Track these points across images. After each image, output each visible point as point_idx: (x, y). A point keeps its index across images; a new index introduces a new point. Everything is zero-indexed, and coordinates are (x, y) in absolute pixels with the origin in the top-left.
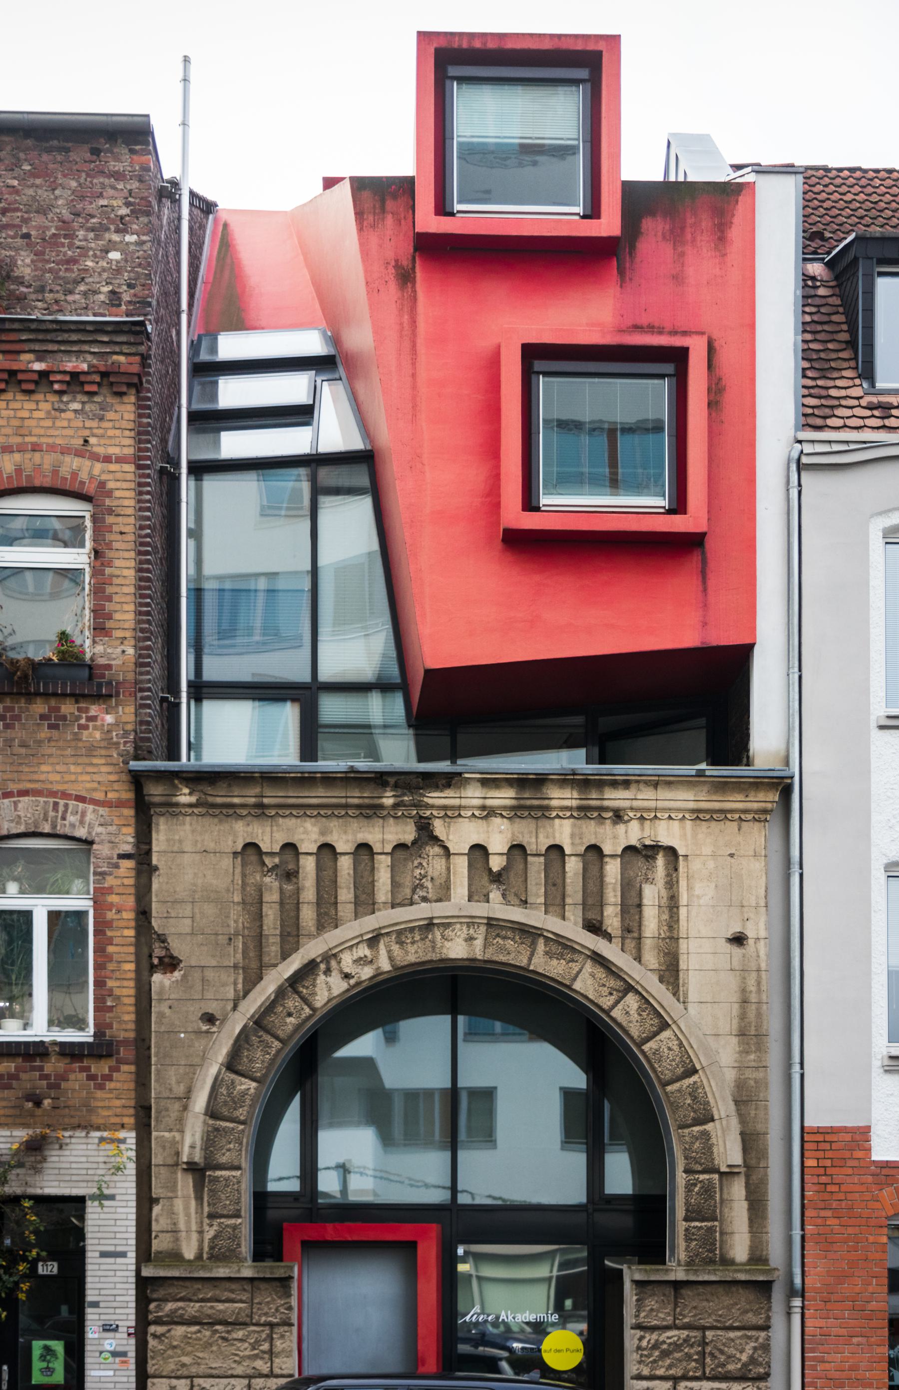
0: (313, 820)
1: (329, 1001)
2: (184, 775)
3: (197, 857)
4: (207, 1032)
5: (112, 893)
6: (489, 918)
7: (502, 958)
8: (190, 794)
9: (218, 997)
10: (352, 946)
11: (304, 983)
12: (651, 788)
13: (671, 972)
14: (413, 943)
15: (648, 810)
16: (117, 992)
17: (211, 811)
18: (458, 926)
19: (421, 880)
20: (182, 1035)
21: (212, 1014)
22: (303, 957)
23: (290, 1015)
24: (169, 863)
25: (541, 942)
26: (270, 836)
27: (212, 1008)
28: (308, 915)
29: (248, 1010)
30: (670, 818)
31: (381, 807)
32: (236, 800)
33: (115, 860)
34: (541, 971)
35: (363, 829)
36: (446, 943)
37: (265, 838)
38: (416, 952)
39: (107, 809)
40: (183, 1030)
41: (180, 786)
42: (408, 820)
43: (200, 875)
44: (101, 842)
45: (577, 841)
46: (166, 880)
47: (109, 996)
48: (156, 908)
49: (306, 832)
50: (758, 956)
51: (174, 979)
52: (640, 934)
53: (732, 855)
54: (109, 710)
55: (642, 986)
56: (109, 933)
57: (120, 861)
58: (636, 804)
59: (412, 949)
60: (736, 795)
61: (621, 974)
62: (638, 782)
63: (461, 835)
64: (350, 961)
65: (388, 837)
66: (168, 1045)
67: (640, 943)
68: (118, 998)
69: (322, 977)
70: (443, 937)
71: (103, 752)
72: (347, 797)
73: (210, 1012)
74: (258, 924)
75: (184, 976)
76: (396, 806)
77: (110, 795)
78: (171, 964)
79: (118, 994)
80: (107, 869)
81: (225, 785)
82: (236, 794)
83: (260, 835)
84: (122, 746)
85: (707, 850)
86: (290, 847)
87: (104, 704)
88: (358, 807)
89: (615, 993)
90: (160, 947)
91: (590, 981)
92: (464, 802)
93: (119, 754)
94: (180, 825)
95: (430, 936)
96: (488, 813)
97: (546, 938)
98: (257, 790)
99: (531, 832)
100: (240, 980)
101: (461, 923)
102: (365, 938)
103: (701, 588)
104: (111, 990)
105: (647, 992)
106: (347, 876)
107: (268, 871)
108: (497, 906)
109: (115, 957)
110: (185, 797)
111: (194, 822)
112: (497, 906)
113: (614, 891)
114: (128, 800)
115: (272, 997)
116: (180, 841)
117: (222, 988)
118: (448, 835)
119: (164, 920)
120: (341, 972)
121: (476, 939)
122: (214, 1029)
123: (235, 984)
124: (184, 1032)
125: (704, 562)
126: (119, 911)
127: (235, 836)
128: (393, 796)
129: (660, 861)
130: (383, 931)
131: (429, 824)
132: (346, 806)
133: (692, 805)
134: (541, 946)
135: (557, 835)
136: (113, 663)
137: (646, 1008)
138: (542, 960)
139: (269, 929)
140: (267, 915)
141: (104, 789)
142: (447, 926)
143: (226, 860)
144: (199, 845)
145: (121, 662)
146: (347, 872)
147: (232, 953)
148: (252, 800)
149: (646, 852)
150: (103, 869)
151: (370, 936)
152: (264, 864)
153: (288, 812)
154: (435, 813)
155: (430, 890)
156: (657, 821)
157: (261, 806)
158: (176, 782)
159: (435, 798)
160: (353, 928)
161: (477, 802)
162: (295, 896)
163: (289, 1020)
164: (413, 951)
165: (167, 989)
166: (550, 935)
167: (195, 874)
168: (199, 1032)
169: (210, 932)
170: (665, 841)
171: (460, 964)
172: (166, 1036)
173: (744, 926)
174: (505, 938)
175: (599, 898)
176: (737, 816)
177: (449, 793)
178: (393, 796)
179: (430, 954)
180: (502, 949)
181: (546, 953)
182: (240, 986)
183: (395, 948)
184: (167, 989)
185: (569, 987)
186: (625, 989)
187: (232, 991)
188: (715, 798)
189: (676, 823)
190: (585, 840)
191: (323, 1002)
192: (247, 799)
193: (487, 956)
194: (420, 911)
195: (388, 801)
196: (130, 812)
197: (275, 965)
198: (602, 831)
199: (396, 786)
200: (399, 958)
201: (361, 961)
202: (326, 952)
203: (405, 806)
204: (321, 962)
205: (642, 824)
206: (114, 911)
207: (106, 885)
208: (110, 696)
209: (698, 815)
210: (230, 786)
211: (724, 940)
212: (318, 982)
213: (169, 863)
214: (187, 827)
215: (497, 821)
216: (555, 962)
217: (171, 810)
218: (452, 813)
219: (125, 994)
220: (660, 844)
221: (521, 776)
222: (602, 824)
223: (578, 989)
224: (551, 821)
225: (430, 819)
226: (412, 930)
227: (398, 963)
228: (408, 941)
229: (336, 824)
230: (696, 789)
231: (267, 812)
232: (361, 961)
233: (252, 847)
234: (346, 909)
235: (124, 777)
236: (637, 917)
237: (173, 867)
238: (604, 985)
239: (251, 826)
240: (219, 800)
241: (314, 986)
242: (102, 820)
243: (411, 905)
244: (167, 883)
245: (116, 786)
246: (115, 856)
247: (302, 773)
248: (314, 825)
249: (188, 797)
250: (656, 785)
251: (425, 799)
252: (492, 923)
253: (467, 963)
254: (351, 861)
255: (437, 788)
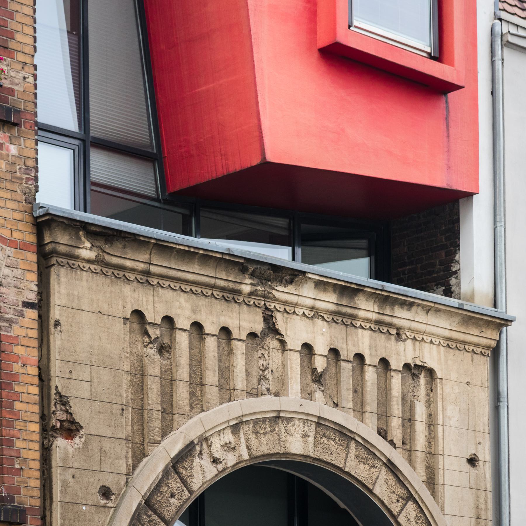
0: (186, 295)
1: (203, 484)
2: (92, 228)
3: (94, 317)
4: (105, 507)
5: (18, 344)
6: (319, 418)
7: (326, 457)
8: (91, 249)
9: (113, 471)
10: (220, 431)
11: (183, 464)
12: (424, 313)
13: (431, 482)
14: (265, 434)
15: (419, 332)
16: (25, 454)
17: (104, 270)
18: (297, 422)
19: (263, 371)
20: (84, 508)
21: (109, 488)
22: (185, 437)
23: (172, 496)
24: (70, 320)
25: (353, 444)
26: (156, 304)
27: (109, 481)
28: (182, 393)
29: (142, 487)
30: (431, 342)
31: (238, 292)
32: (129, 264)
33: (20, 308)
34: (353, 474)
35: (224, 313)
36: (288, 437)
37: (149, 307)
38: (267, 444)
39: (13, 250)
40: (84, 502)
41: (83, 238)
42: (258, 309)
43: (97, 337)
44: (8, 286)
45: (374, 353)
46: (67, 338)
47: (17, 457)
48: (57, 368)
49: (181, 307)
50: (485, 478)
51: (76, 446)
52: (411, 447)
53: (468, 383)
54: (13, 140)
55: (419, 496)
56: (17, 388)
57: (25, 309)
58: (414, 325)
59: (264, 439)
60: (474, 329)
61: (406, 483)
62: (419, 305)
63: (296, 331)
64: (219, 446)
65: (244, 324)
66: (72, 517)
67: (410, 456)
68: (25, 460)
69: (197, 460)
70: (286, 430)
71: (9, 186)
72: (216, 278)
73: (107, 486)
74: (140, 396)
75: (85, 444)
76: (251, 294)
77: (17, 235)
78: (71, 429)
79: (25, 456)
80: (13, 317)
81: (121, 246)
82: (129, 257)
83: (145, 303)
84: (24, 181)
85: (454, 376)
86: (169, 320)
87: (8, 131)
88: (223, 289)
89: (400, 500)
90: (61, 410)
91: (385, 487)
92: (301, 300)
93: (22, 191)
94: (78, 280)
95: (277, 429)
96: (315, 313)
97: (357, 441)
98: (144, 256)
99: (343, 339)
100: (130, 455)
101: (299, 419)
102: (231, 424)
103: (446, 134)
104: (18, 451)
105: (423, 501)
106: (212, 358)
107: (151, 342)
108: (319, 406)
109: (23, 415)
110: (86, 251)
111: (90, 279)
112: (319, 406)
113: (398, 404)
114: (31, 244)
115: (160, 476)
116: (79, 298)
117: (117, 461)
118: (286, 331)
119: (66, 380)
120: (211, 455)
121: (309, 436)
122: (110, 504)
123: (127, 458)
124: (87, 505)
125: (448, 109)
126: (24, 365)
127: (124, 301)
128: (252, 284)
129: (422, 379)
130: (245, 419)
131: (272, 316)
132: (213, 287)
133: (447, 333)
134: (353, 450)
135: (360, 345)
136: (16, 88)
137: (421, 517)
138: (354, 463)
139: (153, 404)
140: (151, 389)
141: (9, 226)
142: (289, 420)
143: (118, 325)
144: (95, 305)
145: (22, 89)
146: (212, 354)
147: (124, 424)
148: (141, 266)
149: (412, 370)
150: (10, 316)
151: (234, 422)
152: (146, 333)
153: (167, 283)
154: (278, 306)
155: (271, 383)
156: (423, 343)
157: (147, 273)
158: (81, 233)
159: (282, 292)
160: (220, 413)
161: (309, 302)
162: (169, 372)
163: (172, 500)
164: (265, 443)
165: (70, 456)
166: (360, 440)
167: (92, 335)
168: (97, 506)
169: (106, 400)
170: (430, 363)
171: (296, 459)
172: (70, 507)
173: (476, 448)
174: (329, 438)
175: (385, 409)
176: (471, 348)
177: (290, 289)
178: (252, 284)
179: (277, 447)
180: (327, 449)
181: (357, 457)
182: (130, 460)
183: (252, 436)
184: (70, 456)
185: (370, 491)
186: (407, 498)
187: (125, 465)
188: (462, 330)
189: (435, 347)
190: (379, 353)
191: (199, 485)
192: (138, 264)
193: (316, 455)
194: (267, 404)
195: (246, 289)
196: (33, 257)
197: (158, 443)
198: (389, 346)
199: (252, 275)
200: (255, 448)
201: (228, 447)
202: (202, 435)
203: (257, 295)
204: (197, 444)
205: (414, 345)
206: (20, 364)
207: (12, 334)
208: (15, 125)
209: (452, 344)
210: (124, 247)
211: (465, 460)
212: (194, 464)
213: (70, 320)
214: (84, 283)
215: (320, 322)
216: (362, 466)
217: (71, 262)
218: (290, 309)
219: (30, 457)
220: (426, 365)
221: (346, 284)
222: (389, 339)
223: (377, 493)
224: (356, 330)
225: (272, 311)
226: (264, 420)
227: (255, 452)
228: (262, 432)
229: (204, 303)
230: (452, 319)
231: (150, 280)
232: (228, 447)
233: (138, 314)
234: (212, 393)
235: (28, 218)
236: (409, 431)
237: (73, 325)
238: (394, 492)
239: (137, 292)
240: (114, 260)
241: (192, 468)
242: (9, 261)
243: (257, 395)
244: (68, 341)
245: (20, 226)
246: (20, 304)
247: (189, 247)
248: (187, 301)
249: (88, 251)
250: (428, 310)
251: (274, 292)
252: (321, 423)
253: (301, 459)
254: (216, 343)
255: (281, 282)
